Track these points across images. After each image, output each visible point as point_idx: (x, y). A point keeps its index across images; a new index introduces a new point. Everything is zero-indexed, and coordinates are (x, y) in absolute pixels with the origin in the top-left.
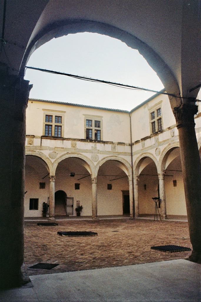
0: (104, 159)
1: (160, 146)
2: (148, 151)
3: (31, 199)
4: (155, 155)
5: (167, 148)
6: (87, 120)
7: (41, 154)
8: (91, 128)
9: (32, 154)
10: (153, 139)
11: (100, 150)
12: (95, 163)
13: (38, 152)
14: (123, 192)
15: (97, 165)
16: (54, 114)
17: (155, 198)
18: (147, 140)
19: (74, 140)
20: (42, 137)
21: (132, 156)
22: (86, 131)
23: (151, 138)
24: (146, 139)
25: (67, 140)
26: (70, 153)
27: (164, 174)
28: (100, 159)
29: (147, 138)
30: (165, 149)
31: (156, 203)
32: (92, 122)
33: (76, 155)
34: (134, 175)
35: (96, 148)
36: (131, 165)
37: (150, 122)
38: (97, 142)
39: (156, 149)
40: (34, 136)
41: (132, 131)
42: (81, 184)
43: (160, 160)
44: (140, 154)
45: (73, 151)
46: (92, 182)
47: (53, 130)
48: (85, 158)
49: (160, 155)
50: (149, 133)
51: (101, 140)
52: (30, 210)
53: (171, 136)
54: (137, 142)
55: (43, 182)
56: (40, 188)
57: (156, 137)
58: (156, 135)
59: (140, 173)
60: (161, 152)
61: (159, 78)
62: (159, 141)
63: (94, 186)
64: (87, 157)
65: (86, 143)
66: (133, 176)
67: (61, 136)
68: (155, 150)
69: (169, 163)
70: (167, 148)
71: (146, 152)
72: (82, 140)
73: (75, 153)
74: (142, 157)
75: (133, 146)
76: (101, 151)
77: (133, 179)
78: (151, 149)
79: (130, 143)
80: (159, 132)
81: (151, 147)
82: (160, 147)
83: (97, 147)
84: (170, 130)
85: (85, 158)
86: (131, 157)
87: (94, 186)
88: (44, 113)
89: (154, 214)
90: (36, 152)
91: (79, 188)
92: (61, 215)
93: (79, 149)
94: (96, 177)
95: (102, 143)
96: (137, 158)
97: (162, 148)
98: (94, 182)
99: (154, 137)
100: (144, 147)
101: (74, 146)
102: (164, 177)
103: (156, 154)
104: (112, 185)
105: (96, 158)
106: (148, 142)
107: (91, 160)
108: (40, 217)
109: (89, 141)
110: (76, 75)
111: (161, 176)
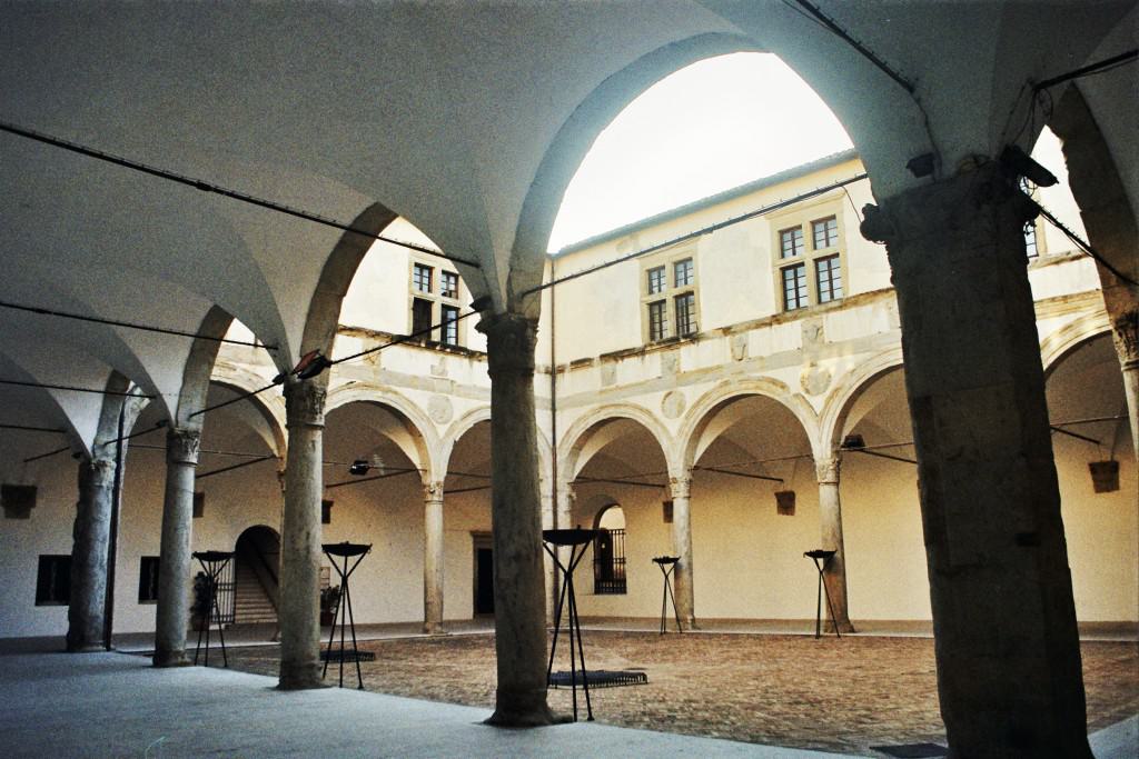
1: (686, 385)
3: (41, 557)
4: (658, 413)
5: (714, 396)
6: (417, 265)
10: (654, 363)
12: (442, 430)
13: (245, 370)
15: (447, 434)
17: (663, 561)
18: (626, 360)
19: (373, 336)
21: (554, 410)
22: (412, 305)
23: (647, 356)
24: (622, 358)
25: (348, 333)
28: (457, 416)
29: (629, 356)
30: (705, 396)
31: (667, 577)
32: (430, 273)
33: (380, 394)
35: (444, 372)
36: (551, 441)
37: (645, 299)
38: (448, 350)
39: (663, 393)
41: (556, 314)
42: (206, 492)
43: (680, 431)
44: (596, 405)
46: (429, 497)
48: (409, 409)
49: (683, 415)
50: (637, 339)
52: (140, 603)
53: (734, 357)
57: (669, 354)
58: (669, 346)
59: (576, 474)
60: (689, 405)
62: (679, 369)
63: (434, 514)
65: (413, 352)
66: (555, 482)
67: (457, 342)
68: (663, 397)
70: (714, 396)
71: (621, 401)
72: (398, 340)
73: (377, 388)
74: (602, 416)
75: (559, 376)
76: (459, 386)
77: (555, 490)
79: (549, 364)
80: (685, 337)
81: (644, 387)
82: (681, 389)
83: (448, 368)
84: (728, 338)
85: (409, 409)
86: (550, 413)
87: (434, 514)
89: (660, 615)
90: (239, 372)
91: (329, 522)
92: (261, 621)
93: (391, 374)
94: (442, 479)
95: (466, 357)
96: (579, 420)
99: (658, 354)
100: (609, 384)
102: (689, 491)
103: (663, 410)
106: (628, 370)
107: (427, 413)
108: (466, 621)
109: (423, 345)
110: (727, 220)
111: (682, 485)
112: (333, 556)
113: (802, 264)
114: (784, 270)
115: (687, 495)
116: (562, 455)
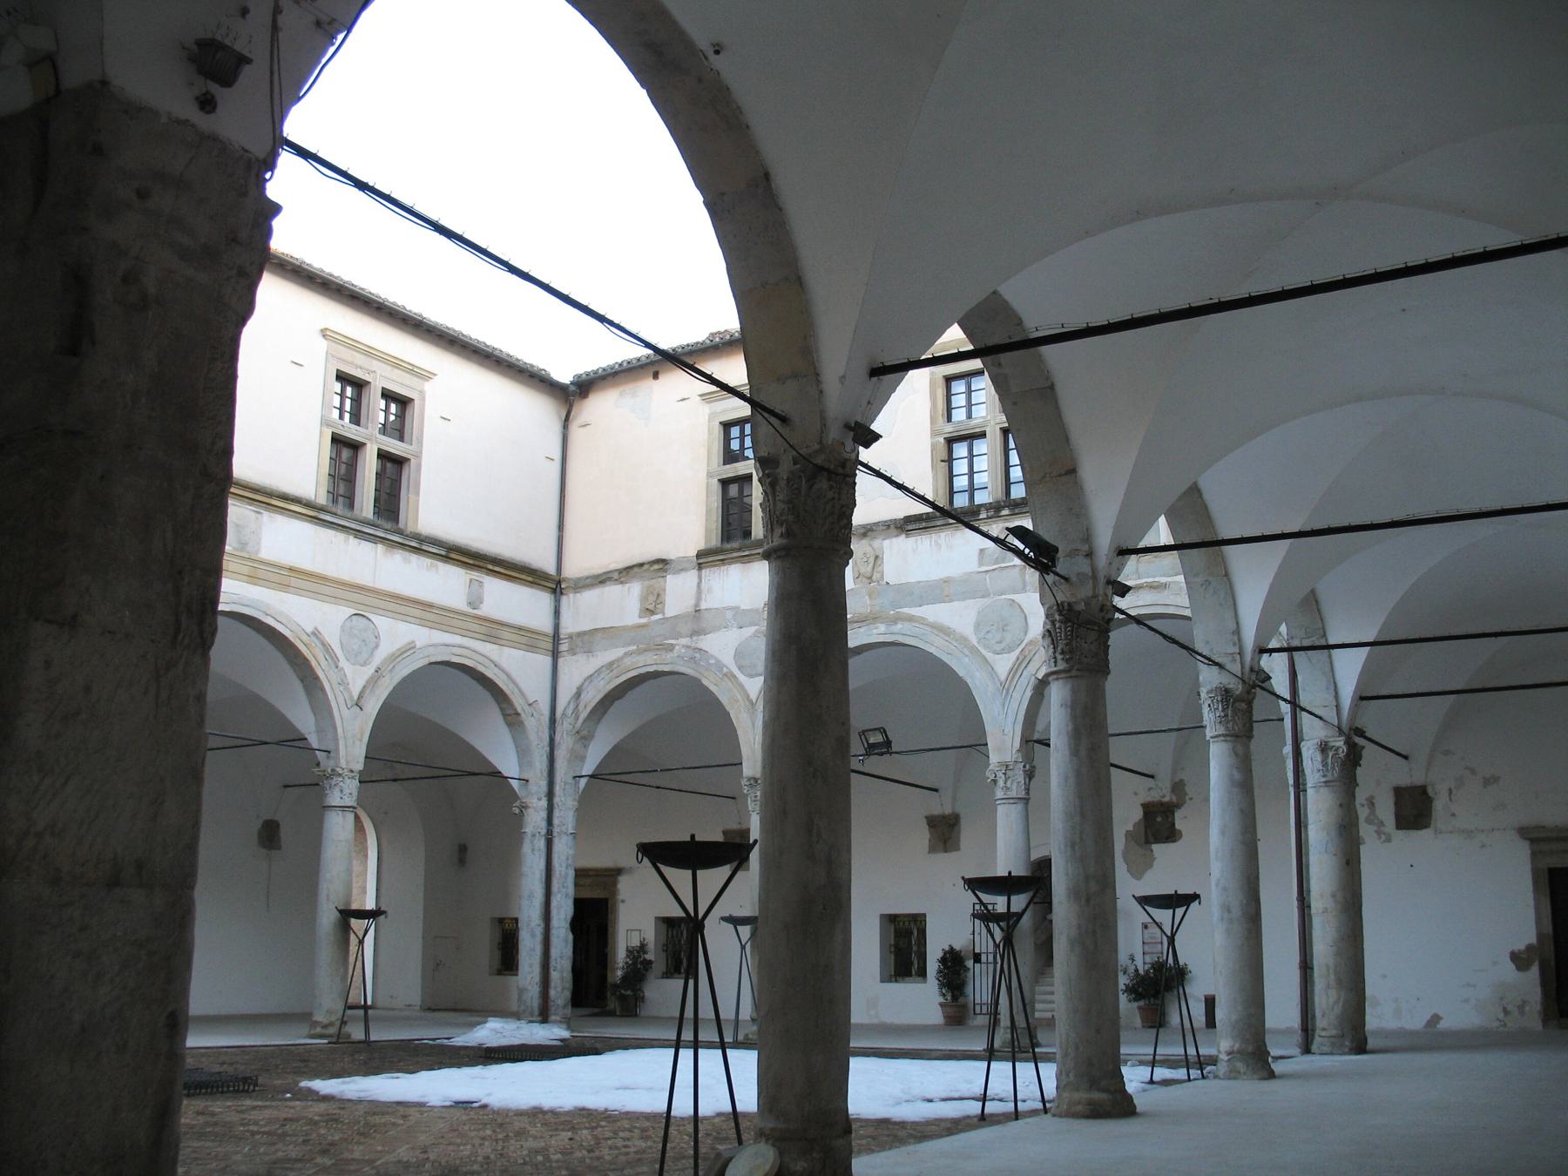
6: (342, 378)
12: (1003, 664)
14: (1533, 841)
15: (1014, 671)
16: (381, 378)
20: (706, 558)
33: (882, 628)
38: (1005, 512)
40: (662, 565)
47: (370, 483)
52: (882, 916)
56: (933, 849)
64: (944, 631)
70: (335, 678)
100: (653, 613)
104: (1430, 791)
107: (974, 641)
112: (666, 870)
113: (983, 435)
114: (950, 441)
115: (1022, 794)
116: (565, 743)
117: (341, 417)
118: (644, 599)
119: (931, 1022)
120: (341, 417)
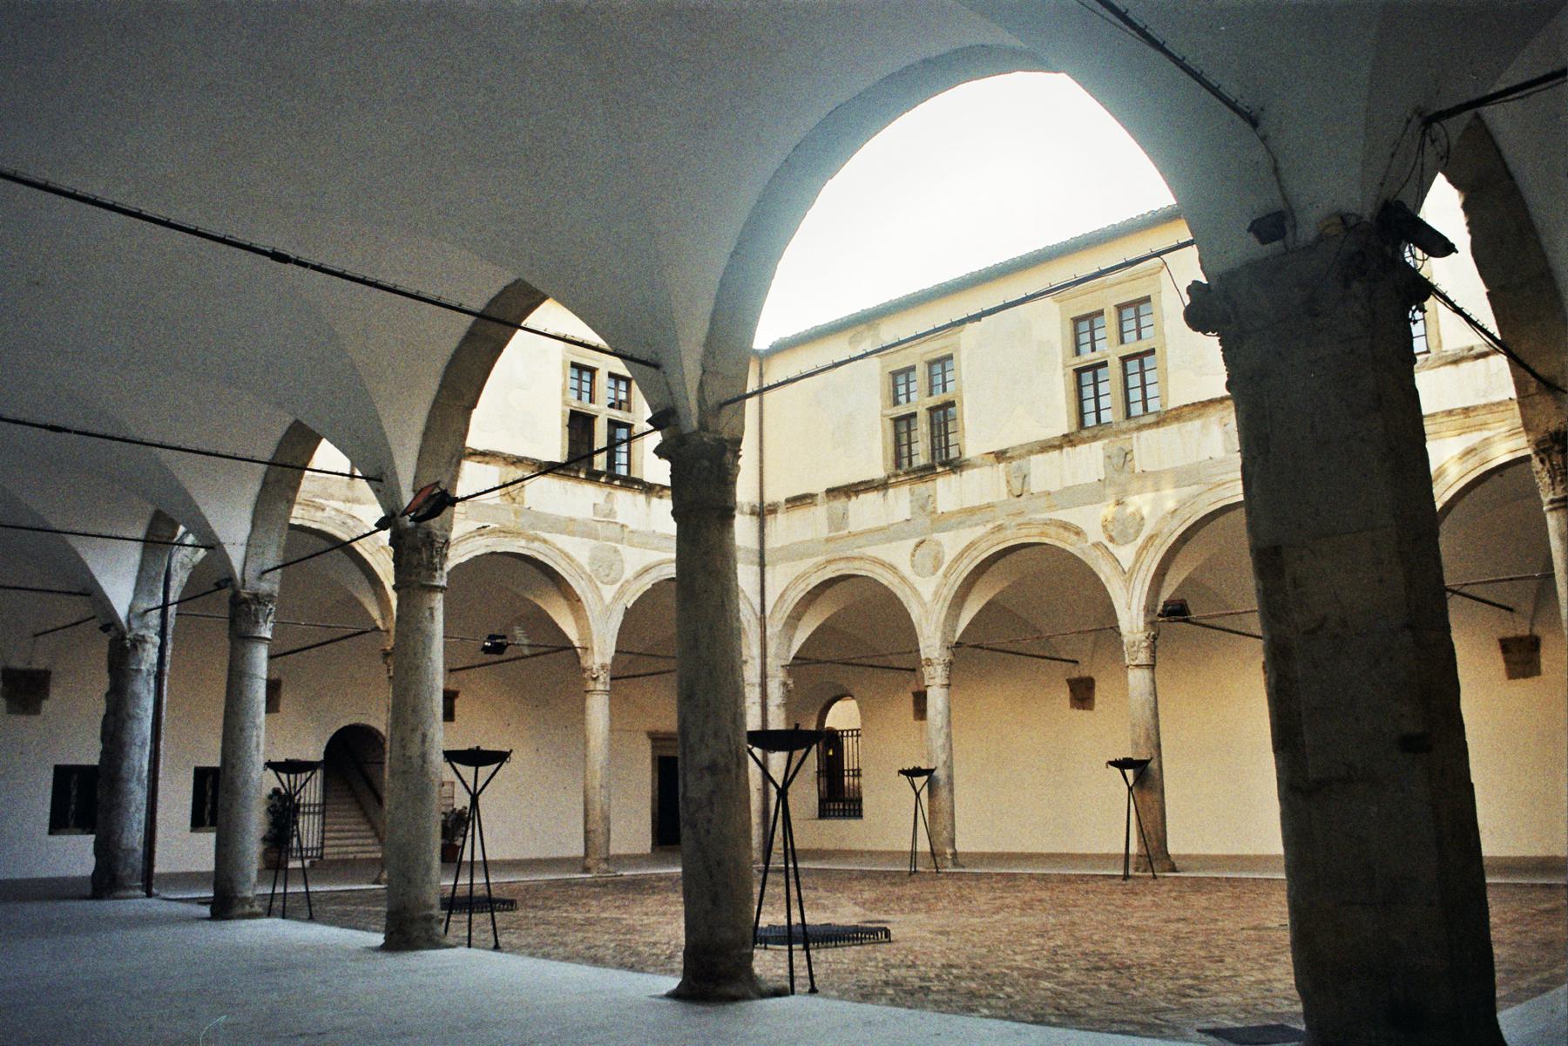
0: (646, 570)
2: (870, 551)
3: (57, 769)
4: (906, 569)
6: (574, 365)
7: (350, 522)
8: (591, 409)
9: (308, 524)
11: (632, 527)
12: (609, 592)
13: (337, 510)
15: (616, 599)
18: (862, 496)
19: (513, 463)
21: (762, 565)
23: (891, 491)
24: (857, 493)
25: (479, 458)
26: (493, 531)
27: (951, 663)
28: (629, 573)
29: (866, 490)
30: (971, 546)
31: (918, 795)
32: (593, 377)
33: (523, 543)
34: (769, 660)
35: (611, 513)
36: (758, 609)
39: (917, 540)
42: (284, 678)
44: (821, 559)
45: (510, 521)
51: (635, 475)
54: (798, 501)
55: (40, 663)
57: (922, 488)
59: (793, 654)
61: (809, 204)
63: (598, 709)
65: (569, 485)
69: (976, 610)
70: (983, 545)
71: (856, 552)
72: (548, 469)
74: (829, 573)
75: (769, 519)
77: (764, 676)
78: (890, 540)
79: (756, 501)
81: (886, 533)
84: (1002, 465)
85: (563, 564)
86: (757, 569)
87: (598, 709)
88: (883, 368)
89: (908, 848)
93: (538, 515)
94: (608, 661)
95: (641, 492)
97: (952, 543)
98: (600, 687)
99: (906, 488)
100: (838, 530)
101: (838, 522)
105: (611, 567)
106: (865, 510)
107: (588, 569)
109: (582, 475)
111: (939, 669)
113: (1105, 364)
114: (1079, 372)
117: (579, 398)
118: (830, 518)
119: (638, 851)
120: (579, 398)
